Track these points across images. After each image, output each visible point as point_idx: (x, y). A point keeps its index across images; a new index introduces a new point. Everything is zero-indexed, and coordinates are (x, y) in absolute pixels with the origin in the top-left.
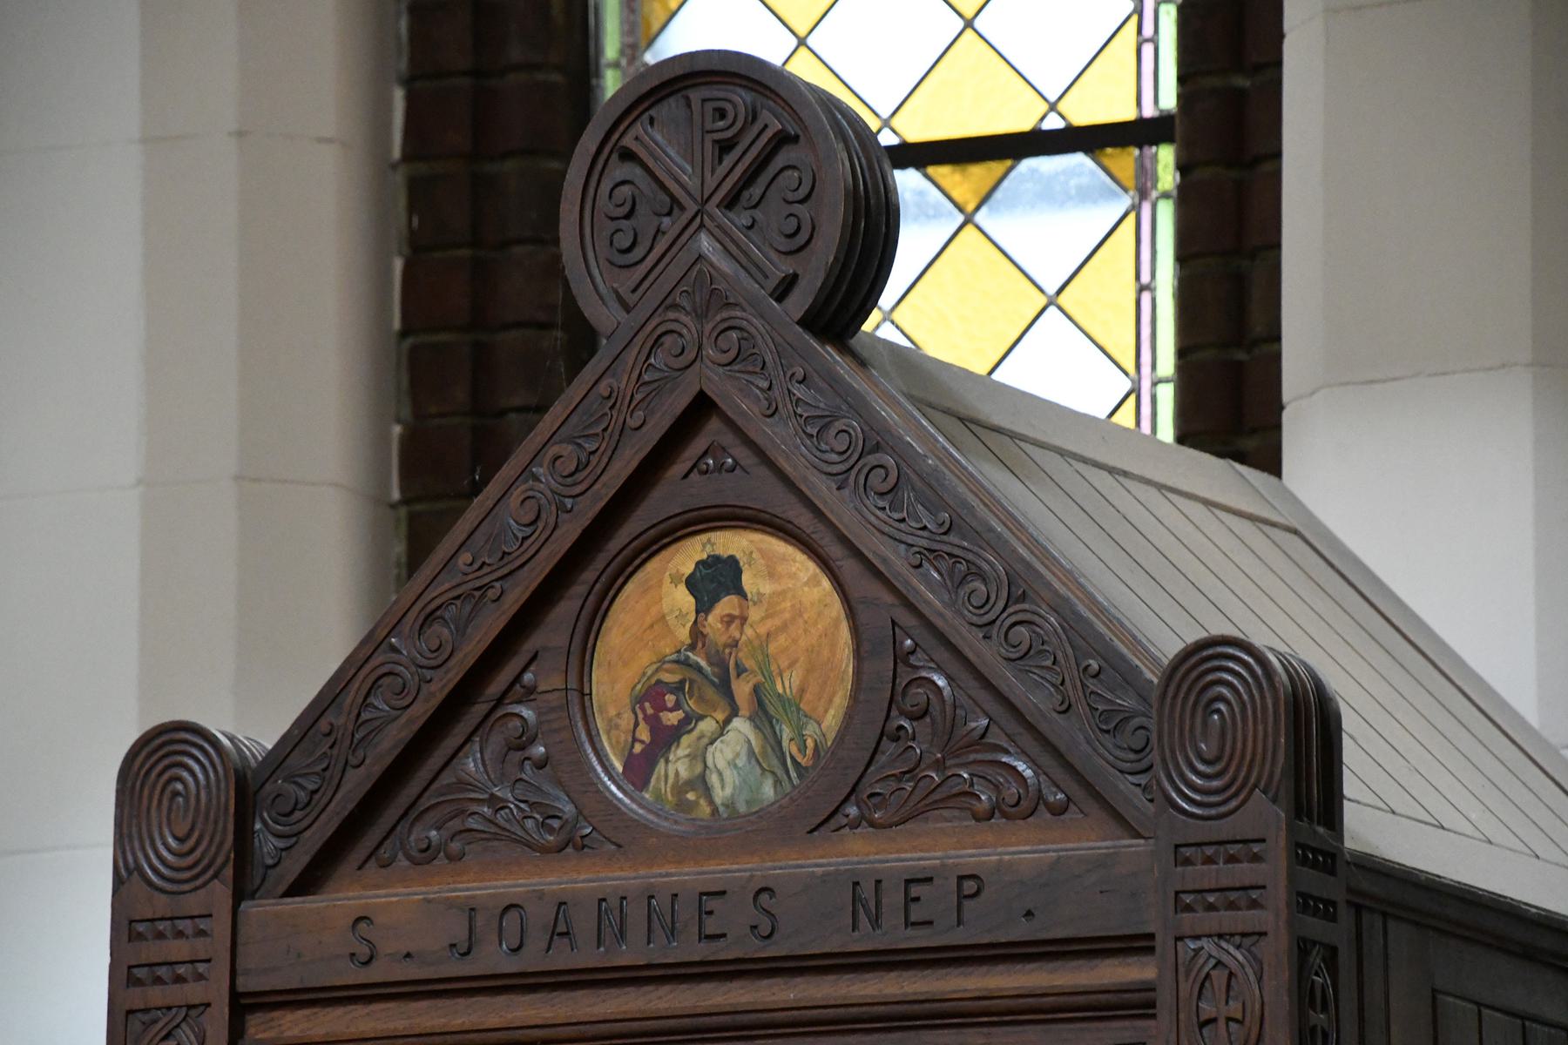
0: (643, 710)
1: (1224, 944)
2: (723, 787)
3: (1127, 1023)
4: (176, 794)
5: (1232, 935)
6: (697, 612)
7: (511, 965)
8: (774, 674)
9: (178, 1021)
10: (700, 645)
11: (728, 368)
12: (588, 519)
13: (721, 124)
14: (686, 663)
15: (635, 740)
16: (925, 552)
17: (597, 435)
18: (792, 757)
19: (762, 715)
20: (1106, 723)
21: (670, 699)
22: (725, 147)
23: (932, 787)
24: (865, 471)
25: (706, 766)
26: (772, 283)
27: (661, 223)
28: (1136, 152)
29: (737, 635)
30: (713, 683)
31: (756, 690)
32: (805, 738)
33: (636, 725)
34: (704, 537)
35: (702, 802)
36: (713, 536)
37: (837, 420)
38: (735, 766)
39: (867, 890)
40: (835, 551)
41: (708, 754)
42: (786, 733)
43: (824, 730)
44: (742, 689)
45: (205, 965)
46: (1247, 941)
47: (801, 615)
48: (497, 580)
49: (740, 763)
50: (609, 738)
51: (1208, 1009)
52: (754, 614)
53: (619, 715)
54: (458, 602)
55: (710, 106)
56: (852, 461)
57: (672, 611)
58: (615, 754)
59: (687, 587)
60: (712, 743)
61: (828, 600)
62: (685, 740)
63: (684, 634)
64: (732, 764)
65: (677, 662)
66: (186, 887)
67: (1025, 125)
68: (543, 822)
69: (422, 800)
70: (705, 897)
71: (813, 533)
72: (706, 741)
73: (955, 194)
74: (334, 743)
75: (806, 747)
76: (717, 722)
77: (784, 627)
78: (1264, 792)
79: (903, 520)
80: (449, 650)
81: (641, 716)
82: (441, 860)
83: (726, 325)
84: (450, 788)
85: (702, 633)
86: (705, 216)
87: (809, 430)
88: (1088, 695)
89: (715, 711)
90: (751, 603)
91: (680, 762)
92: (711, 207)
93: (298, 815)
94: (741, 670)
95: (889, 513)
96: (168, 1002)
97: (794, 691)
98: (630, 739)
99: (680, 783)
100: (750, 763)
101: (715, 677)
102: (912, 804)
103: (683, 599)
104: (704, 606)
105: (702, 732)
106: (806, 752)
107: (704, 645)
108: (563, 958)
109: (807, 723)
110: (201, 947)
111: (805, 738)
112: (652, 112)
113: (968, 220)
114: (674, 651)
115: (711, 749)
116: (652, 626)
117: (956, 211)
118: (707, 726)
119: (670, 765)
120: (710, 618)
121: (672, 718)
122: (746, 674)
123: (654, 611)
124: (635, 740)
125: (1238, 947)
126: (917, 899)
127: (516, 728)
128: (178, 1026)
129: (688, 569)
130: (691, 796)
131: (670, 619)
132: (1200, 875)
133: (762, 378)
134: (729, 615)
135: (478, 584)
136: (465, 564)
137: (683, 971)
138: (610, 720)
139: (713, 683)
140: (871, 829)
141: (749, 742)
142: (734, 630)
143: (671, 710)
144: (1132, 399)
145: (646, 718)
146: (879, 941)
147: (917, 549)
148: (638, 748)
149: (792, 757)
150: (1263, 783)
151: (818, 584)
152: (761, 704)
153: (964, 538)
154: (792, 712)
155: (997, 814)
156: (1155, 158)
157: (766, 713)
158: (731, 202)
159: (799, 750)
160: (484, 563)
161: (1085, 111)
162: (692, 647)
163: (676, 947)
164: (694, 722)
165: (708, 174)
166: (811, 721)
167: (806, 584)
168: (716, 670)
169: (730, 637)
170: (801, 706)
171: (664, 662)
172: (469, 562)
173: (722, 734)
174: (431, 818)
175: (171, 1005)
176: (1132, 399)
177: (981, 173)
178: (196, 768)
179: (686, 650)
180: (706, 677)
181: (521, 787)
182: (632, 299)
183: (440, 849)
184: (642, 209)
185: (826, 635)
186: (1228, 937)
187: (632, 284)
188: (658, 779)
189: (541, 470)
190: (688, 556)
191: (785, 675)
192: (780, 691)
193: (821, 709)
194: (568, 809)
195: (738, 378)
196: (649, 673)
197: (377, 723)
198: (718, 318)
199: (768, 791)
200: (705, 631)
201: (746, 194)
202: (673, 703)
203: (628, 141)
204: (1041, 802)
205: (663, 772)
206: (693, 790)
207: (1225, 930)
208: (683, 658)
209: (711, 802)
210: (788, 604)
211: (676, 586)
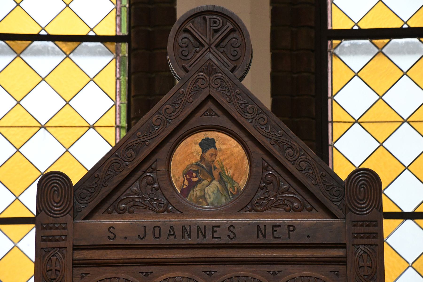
0: (186, 177)
1: (366, 247)
2: (210, 198)
3: (333, 266)
4: (55, 190)
5: (368, 245)
6: (202, 152)
7: (157, 242)
8: (225, 170)
9: (57, 251)
10: (203, 161)
11: (217, 89)
12: (176, 126)
13: (214, 25)
14: (199, 165)
15: (184, 185)
16: (276, 141)
17: (179, 104)
18: (230, 192)
19: (222, 179)
20: (328, 188)
21: (194, 175)
22: (216, 31)
23: (274, 202)
24: (258, 119)
25: (205, 193)
26: (230, 68)
27: (196, 50)
28: (116, 44)
29: (214, 159)
30: (207, 171)
31: (220, 174)
32: (234, 187)
33: (184, 180)
34: (204, 133)
35: (204, 202)
36: (207, 133)
37: (249, 105)
38: (214, 193)
39: (262, 227)
40: (245, 139)
41: (205, 190)
42: (229, 186)
43: (240, 185)
44: (216, 173)
46: (372, 247)
47: (233, 155)
48: (148, 140)
49: (215, 192)
50: (176, 184)
51: (361, 264)
52: (219, 154)
53: (179, 178)
54: (137, 145)
55: (212, 20)
56: (254, 116)
57: (195, 152)
58: (178, 188)
59: (199, 145)
60: (207, 187)
61: (241, 152)
62: (199, 185)
63: (198, 158)
64: (213, 193)
65: (197, 165)
66: (59, 216)
67: (35, 32)
68: (158, 204)
69: (122, 196)
70: (213, 227)
71: (239, 134)
72: (205, 186)
73: (64, 49)
74: (99, 180)
75: (235, 190)
76: (208, 181)
77: (228, 158)
78: (377, 209)
79: (269, 132)
80: (134, 157)
81: (185, 178)
82: (127, 212)
83: (217, 78)
84: (129, 194)
85: (204, 158)
86: (211, 49)
87: (241, 107)
89: (207, 179)
90: (218, 151)
91: (197, 191)
92: (212, 46)
93: (87, 198)
94: (215, 168)
95: (265, 130)
96: (54, 246)
97: (231, 175)
98: (182, 184)
99: (197, 197)
100: (218, 192)
101: (208, 169)
102: (268, 206)
103: (198, 149)
104: (204, 150)
105: (204, 183)
106: (234, 191)
107: (204, 161)
108: (172, 241)
109: (235, 183)
110: (64, 232)
111: (234, 187)
112: (193, 20)
113: (68, 56)
114: (195, 162)
115: (206, 189)
116: (189, 155)
117: (64, 54)
118: (205, 182)
119: (194, 192)
120: (206, 154)
121: (195, 179)
122: (216, 170)
123: (189, 151)
124: (184, 185)
125: (370, 248)
126: (276, 231)
127: (150, 179)
128: (57, 253)
129: (200, 141)
130: (200, 200)
131: (195, 154)
132: (358, 229)
133: (228, 92)
134: (211, 154)
135: (143, 140)
136: (139, 135)
138: (176, 179)
139: (207, 171)
140: (256, 212)
141: (218, 187)
142: (213, 158)
143: (195, 177)
144: (114, 106)
145: (187, 179)
146: (205, 242)
147: (273, 140)
148: (185, 187)
149: (230, 192)
150: (376, 206)
151: (238, 147)
152: (221, 178)
153: (286, 138)
154: (230, 180)
155: (292, 210)
156: (121, 46)
157: (223, 180)
158: (217, 46)
159: (233, 190)
160: (145, 135)
161: (101, 32)
162: (201, 161)
163: (198, 240)
164: (201, 181)
165: (211, 38)
166: (236, 183)
167: (234, 147)
168: (208, 168)
169: (212, 160)
170: (233, 179)
171: (192, 165)
172: (139, 135)
173: (210, 185)
174: (124, 201)
175: (55, 247)
176: (114, 106)
177: (71, 45)
179: (199, 162)
180: (205, 169)
181: (152, 195)
182: (189, 69)
183: (127, 210)
184: (190, 46)
185: (240, 160)
186: (367, 245)
187: (189, 65)
188: (191, 195)
189: (161, 112)
190: (200, 136)
191: (228, 170)
192: (227, 174)
193: (239, 180)
194: (165, 202)
195: (220, 92)
196: (188, 167)
197: (112, 175)
198: (214, 76)
199: (223, 200)
200: (205, 157)
201: (222, 44)
202: (195, 176)
203: (188, 27)
204: (305, 208)
205: (192, 194)
206: (201, 199)
207: (366, 243)
208: (198, 164)
209: (207, 202)
210: (229, 152)
211: (196, 145)
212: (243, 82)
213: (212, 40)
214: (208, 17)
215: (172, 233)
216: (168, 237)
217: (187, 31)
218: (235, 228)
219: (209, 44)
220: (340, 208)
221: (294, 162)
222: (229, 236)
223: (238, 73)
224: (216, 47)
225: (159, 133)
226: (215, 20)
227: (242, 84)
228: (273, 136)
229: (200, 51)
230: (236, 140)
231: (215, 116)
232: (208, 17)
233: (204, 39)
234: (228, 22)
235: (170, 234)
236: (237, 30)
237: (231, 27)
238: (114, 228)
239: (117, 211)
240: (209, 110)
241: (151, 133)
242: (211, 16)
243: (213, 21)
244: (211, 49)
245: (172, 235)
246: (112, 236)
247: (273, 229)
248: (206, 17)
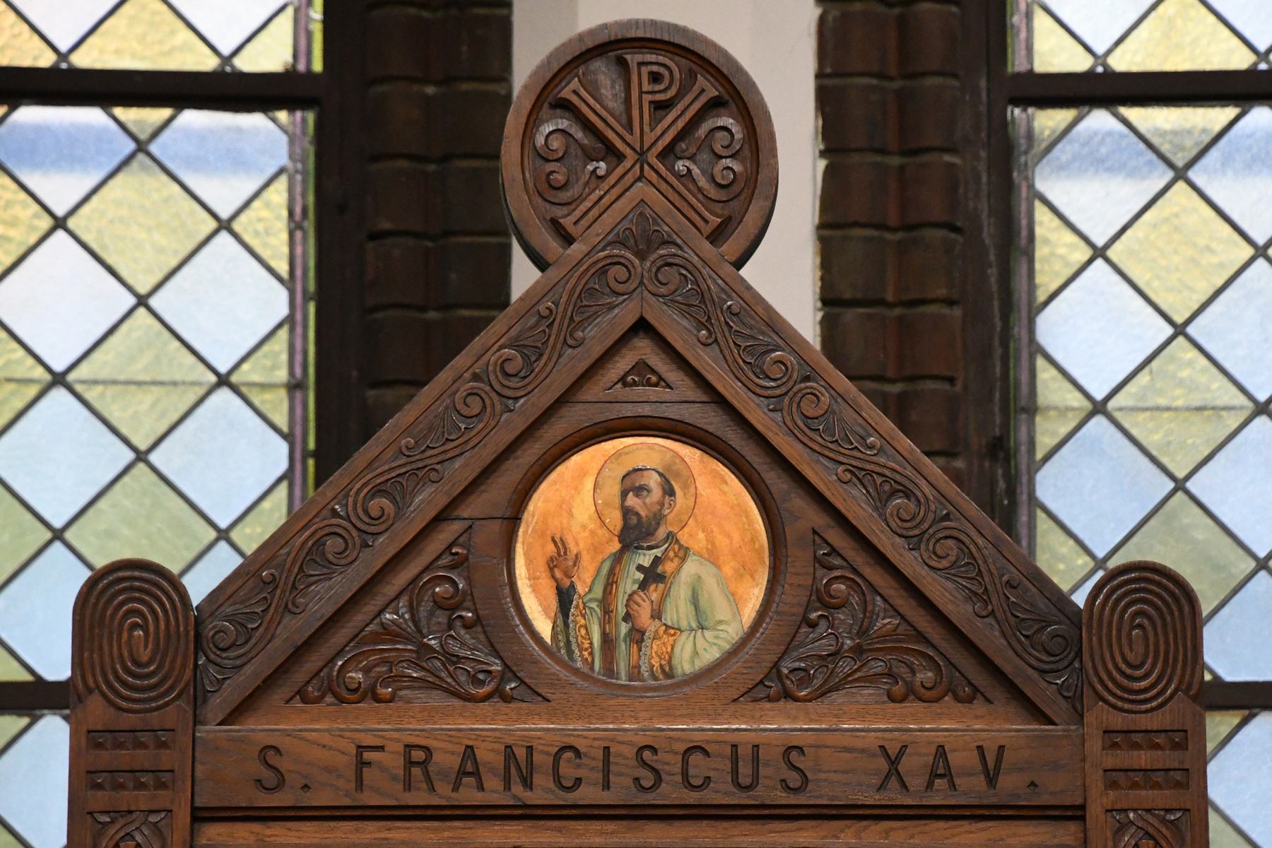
4: (135, 626)
13: (658, 87)
22: (661, 107)
26: (707, 229)
39: (521, 753)
45: (168, 775)
48: (438, 463)
55: (645, 70)
88: (308, 558)
108: (469, 795)
137: (596, 812)
146: (477, 798)
158: (662, 156)
178: (1119, 659)
187: (573, 218)
203: (566, 93)
212: (744, 272)
213: (649, 138)
214: (633, 59)
215: (469, 767)
216: (930, 785)
217: (564, 106)
219: (638, 149)
220: (1066, 694)
221: (915, 542)
222: (637, 779)
223: (732, 247)
224: (663, 158)
225: (477, 441)
226: (655, 68)
227: (743, 280)
228: (847, 452)
229: (609, 173)
231: (656, 385)
232: (633, 59)
233: (646, 129)
234: (699, 75)
235: (934, 775)
236: (730, 101)
237: (712, 93)
238: (654, 750)
239: (336, 695)
240: (642, 368)
242: (640, 57)
243: (651, 73)
244: (646, 167)
245: (941, 776)
246: (794, 779)
247: (359, 754)
248: (628, 57)
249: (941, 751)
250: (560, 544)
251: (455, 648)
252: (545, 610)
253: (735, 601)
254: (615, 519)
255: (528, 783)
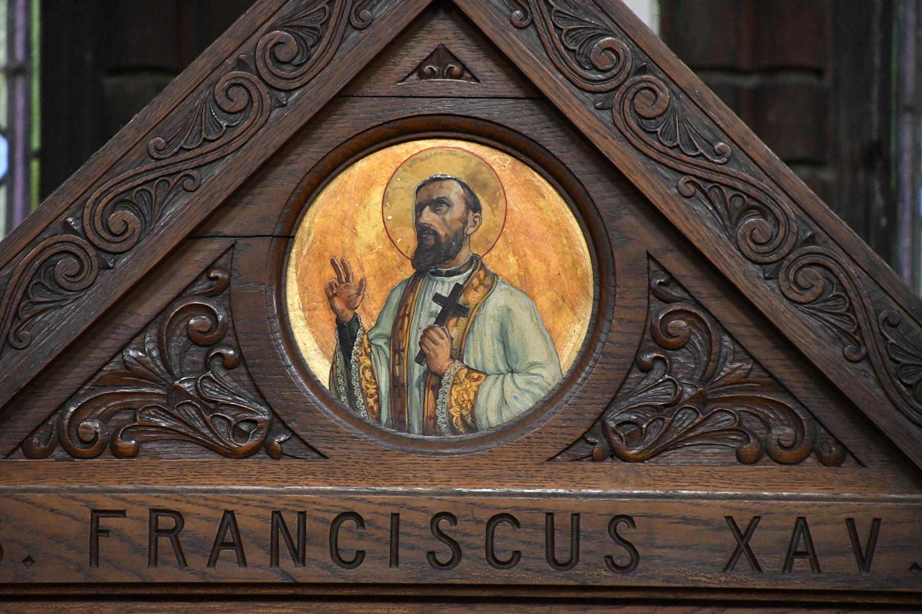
39: (291, 520)
48: (193, 169)
146: (304, 574)
160: (181, 148)
194: (263, 416)
216: (788, 565)
218: (634, 526)
222: (431, 554)
230: (335, 177)
231: (459, 77)
235: (792, 554)
240: (442, 55)
241: (205, 140)
246: (622, 556)
249: (802, 524)
250: (341, 268)
251: (212, 392)
252: (323, 348)
253: (552, 338)
254: (408, 238)
255: (299, 557)
